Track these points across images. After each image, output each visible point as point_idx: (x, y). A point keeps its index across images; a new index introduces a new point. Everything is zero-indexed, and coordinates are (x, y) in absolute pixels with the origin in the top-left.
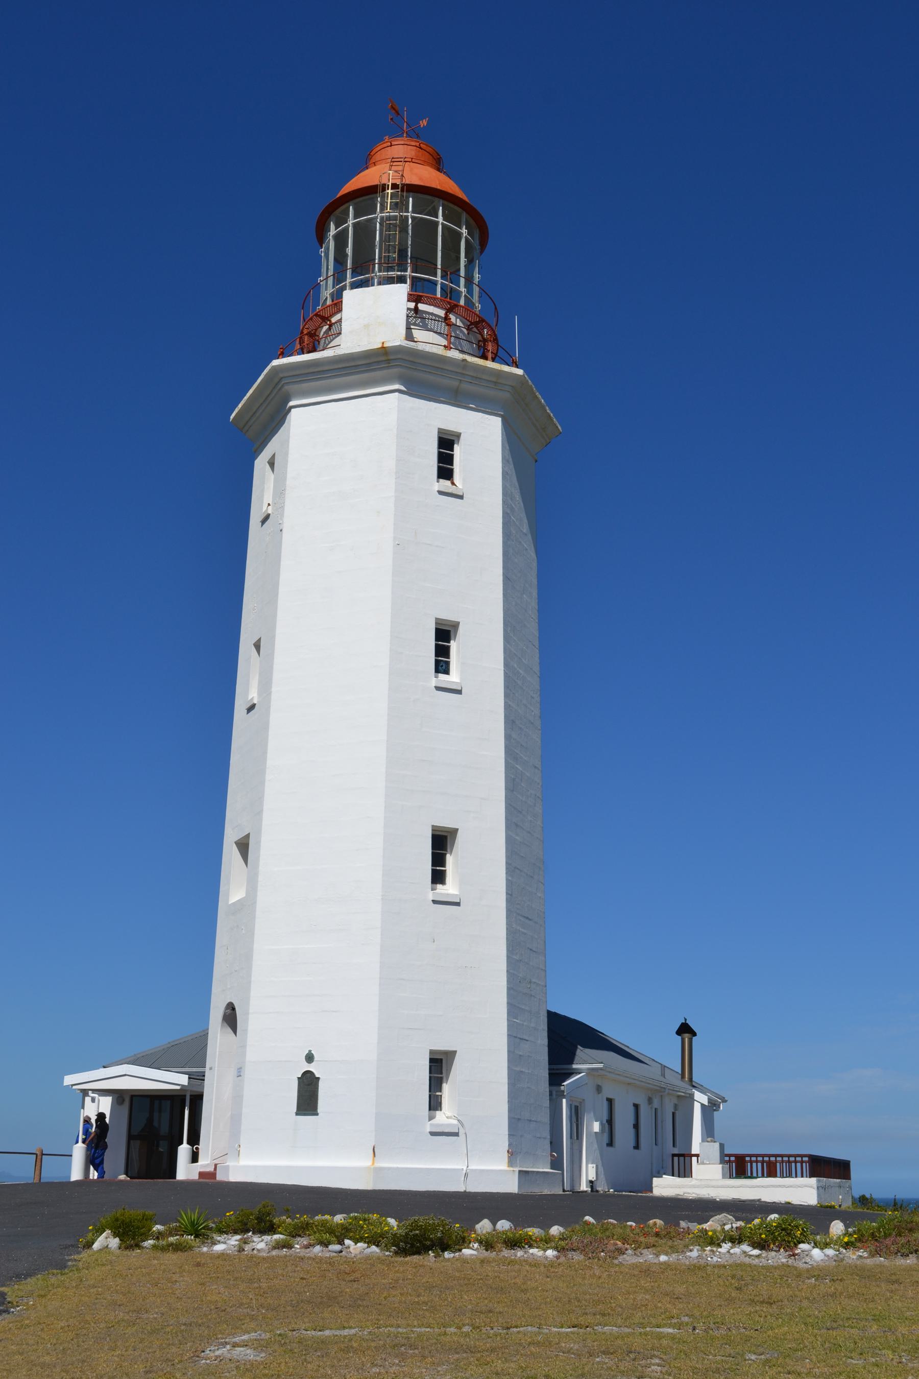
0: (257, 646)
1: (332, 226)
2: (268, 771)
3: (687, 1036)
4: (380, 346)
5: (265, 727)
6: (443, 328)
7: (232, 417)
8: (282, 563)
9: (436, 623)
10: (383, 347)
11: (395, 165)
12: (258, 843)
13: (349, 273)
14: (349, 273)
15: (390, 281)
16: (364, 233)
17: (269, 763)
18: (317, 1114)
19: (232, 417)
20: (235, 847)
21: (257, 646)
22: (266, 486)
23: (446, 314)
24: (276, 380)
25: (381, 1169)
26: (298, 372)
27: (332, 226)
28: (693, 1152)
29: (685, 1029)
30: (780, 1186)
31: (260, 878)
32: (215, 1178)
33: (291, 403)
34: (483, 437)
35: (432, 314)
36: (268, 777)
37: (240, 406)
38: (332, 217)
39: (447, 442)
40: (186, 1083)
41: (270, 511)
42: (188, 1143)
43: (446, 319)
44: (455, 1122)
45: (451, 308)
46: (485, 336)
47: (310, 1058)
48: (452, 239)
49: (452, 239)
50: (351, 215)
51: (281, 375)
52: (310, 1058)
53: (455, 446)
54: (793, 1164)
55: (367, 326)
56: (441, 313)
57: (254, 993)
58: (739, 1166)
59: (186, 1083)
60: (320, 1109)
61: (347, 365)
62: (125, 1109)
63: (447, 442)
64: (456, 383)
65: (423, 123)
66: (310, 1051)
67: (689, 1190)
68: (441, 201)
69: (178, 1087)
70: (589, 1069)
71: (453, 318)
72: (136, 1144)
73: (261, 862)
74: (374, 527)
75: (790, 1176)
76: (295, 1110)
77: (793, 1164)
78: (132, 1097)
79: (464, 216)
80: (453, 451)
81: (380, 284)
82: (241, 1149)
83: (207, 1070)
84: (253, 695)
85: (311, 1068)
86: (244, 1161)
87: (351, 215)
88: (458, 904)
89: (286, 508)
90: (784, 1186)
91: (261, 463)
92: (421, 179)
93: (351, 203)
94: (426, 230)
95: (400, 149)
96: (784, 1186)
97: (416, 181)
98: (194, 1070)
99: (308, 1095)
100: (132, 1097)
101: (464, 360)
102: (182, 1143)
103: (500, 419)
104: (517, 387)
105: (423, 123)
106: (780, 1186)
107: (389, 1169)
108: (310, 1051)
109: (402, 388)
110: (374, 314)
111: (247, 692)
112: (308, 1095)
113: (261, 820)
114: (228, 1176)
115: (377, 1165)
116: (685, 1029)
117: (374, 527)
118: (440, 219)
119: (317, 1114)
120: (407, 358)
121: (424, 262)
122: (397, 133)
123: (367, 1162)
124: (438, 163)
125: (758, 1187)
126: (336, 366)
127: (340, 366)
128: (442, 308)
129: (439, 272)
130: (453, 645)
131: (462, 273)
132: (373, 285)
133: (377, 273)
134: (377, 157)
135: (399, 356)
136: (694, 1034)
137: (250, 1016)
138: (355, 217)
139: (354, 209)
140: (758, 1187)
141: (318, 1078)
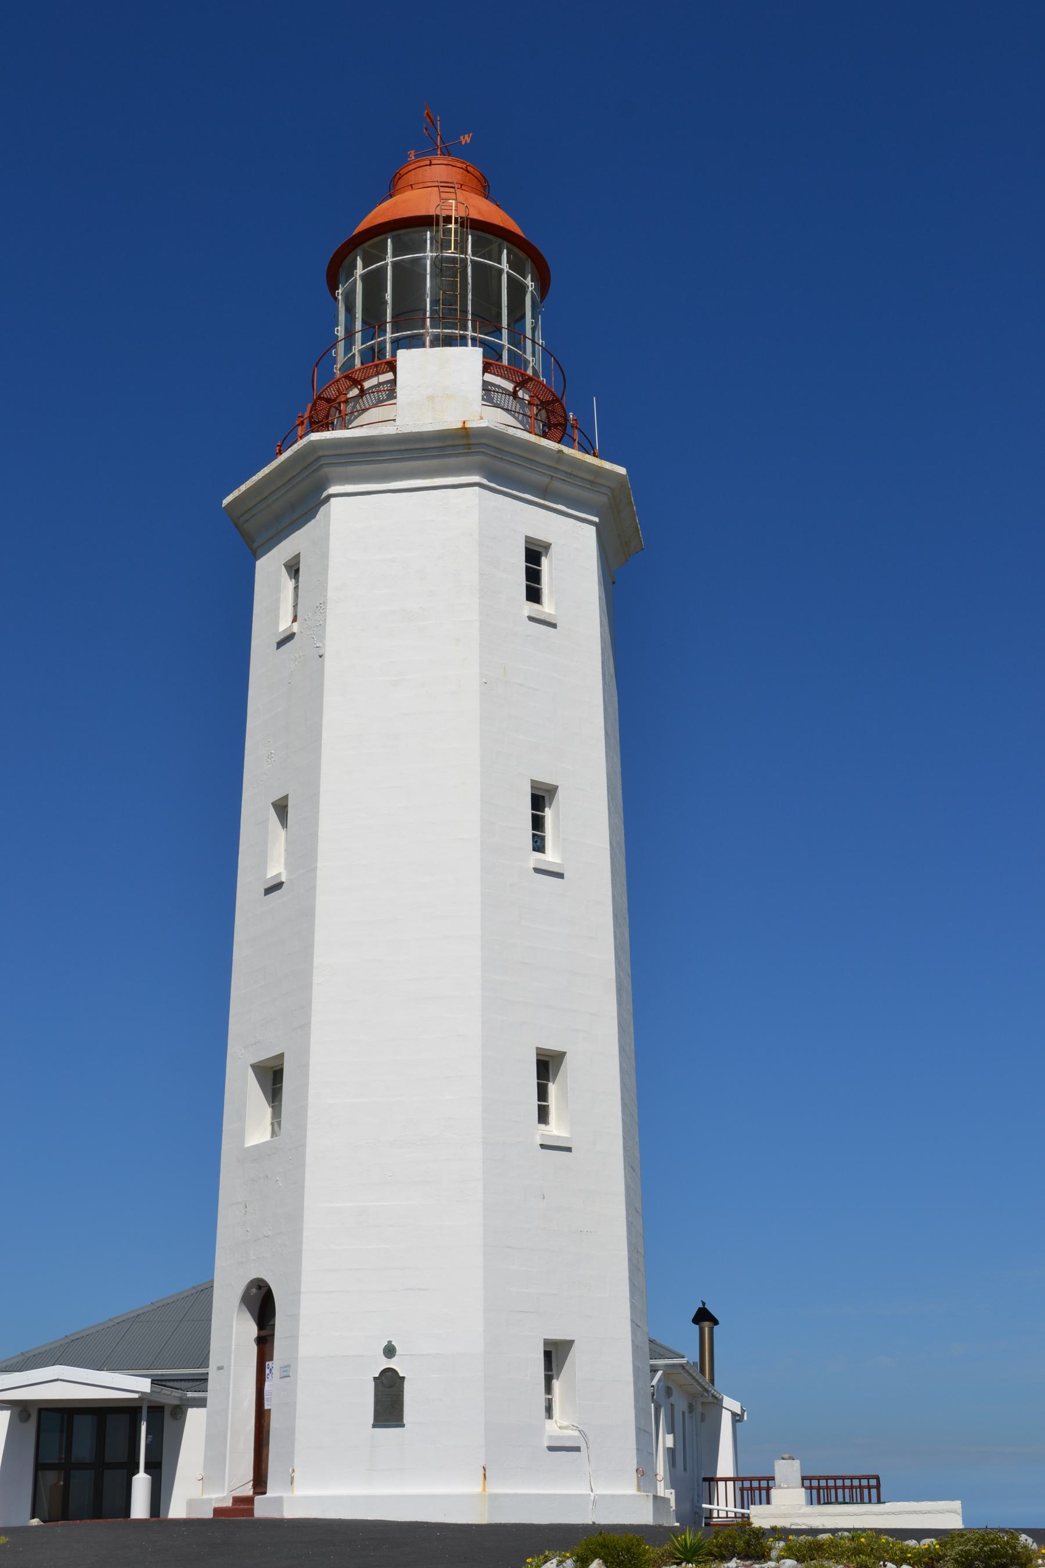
0: (281, 808)
1: (359, 262)
2: (315, 971)
3: (707, 1325)
4: (460, 425)
5: (309, 914)
6: (510, 402)
7: (226, 502)
8: (325, 699)
9: (532, 787)
10: (464, 428)
11: (435, 190)
12: (304, 1068)
13: (389, 327)
14: (389, 327)
15: (449, 341)
16: (408, 277)
17: (317, 961)
18: (403, 1426)
19: (226, 502)
20: (250, 1069)
21: (281, 808)
22: (282, 595)
23: (515, 388)
24: (311, 459)
25: (496, 1496)
26: (343, 452)
27: (359, 262)
28: (719, 1475)
29: (703, 1316)
30: (915, 1512)
31: (310, 1113)
32: (252, 1514)
33: (333, 490)
34: (575, 547)
35: (499, 387)
36: (317, 979)
37: (243, 488)
38: (359, 250)
39: (534, 554)
40: (148, 1390)
41: (295, 628)
42: (146, 1472)
43: (514, 394)
44: (576, 1433)
45: (522, 383)
46: (552, 416)
47: (390, 1351)
48: (517, 290)
49: (517, 290)
50: (389, 251)
51: (321, 453)
52: (390, 1351)
53: (543, 559)
54: (757, 1492)
55: (431, 398)
56: (509, 386)
57: (307, 1266)
58: (821, 1489)
59: (148, 1390)
60: (407, 1418)
61: (413, 447)
62: (31, 1428)
63: (534, 554)
64: (545, 480)
65: (466, 139)
66: (390, 1342)
67: (798, 1520)
68: (505, 244)
69: (136, 1396)
70: (666, 1365)
71: (520, 394)
72: (52, 1478)
73: (311, 1092)
74: (430, 654)
75: (862, 1502)
76: (371, 1421)
77: (757, 1492)
78: (40, 1410)
79: (529, 265)
80: (539, 565)
81: (433, 345)
82: (296, 1475)
83: (212, 1371)
84: (276, 869)
85: (392, 1364)
86: (300, 1491)
87: (389, 251)
88: (569, 1149)
89: (328, 628)
90: (921, 1512)
91: (269, 568)
92: (480, 213)
93: (389, 235)
94: (486, 278)
95: (440, 170)
96: (921, 1512)
97: (474, 215)
98: (159, 1372)
99: (389, 1400)
100: (40, 1410)
101: (560, 451)
102: (136, 1471)
103: (594, 528)
104: (616, 489)
105: (466, 139)
106: (915, 1512)
107: (506, 1495)
108: (390, 1342)
109: (485, 482)
110: (441, 384)
111: (263, 864)
112: (389, 1400)
113: (308, 1035)
114: (282, 1511)
115: (494, 1489)
116: (703, 1316)
117: (430, 654)
118: (505, 266)
119: (403, 1426)
120: (492, 443)
121: (488, 322)
122: (427, 150)
123: (477, 1489)
124: (485, 190)
125: (887, 1514)
126: (397, 448)
127: (403, 447)
128: (512, 381)
129: (505, 332)
130: (548, 814)
131: (529, 334)
132: (423, 346)
133: (430, 331)
134: (411, 178)
135: (483, 441)
136: (716, 1322)
137: (303, 1297)
138: (394, 256)
139: (393, 242)
140: (887, 1514)
141: (404, 1378)
